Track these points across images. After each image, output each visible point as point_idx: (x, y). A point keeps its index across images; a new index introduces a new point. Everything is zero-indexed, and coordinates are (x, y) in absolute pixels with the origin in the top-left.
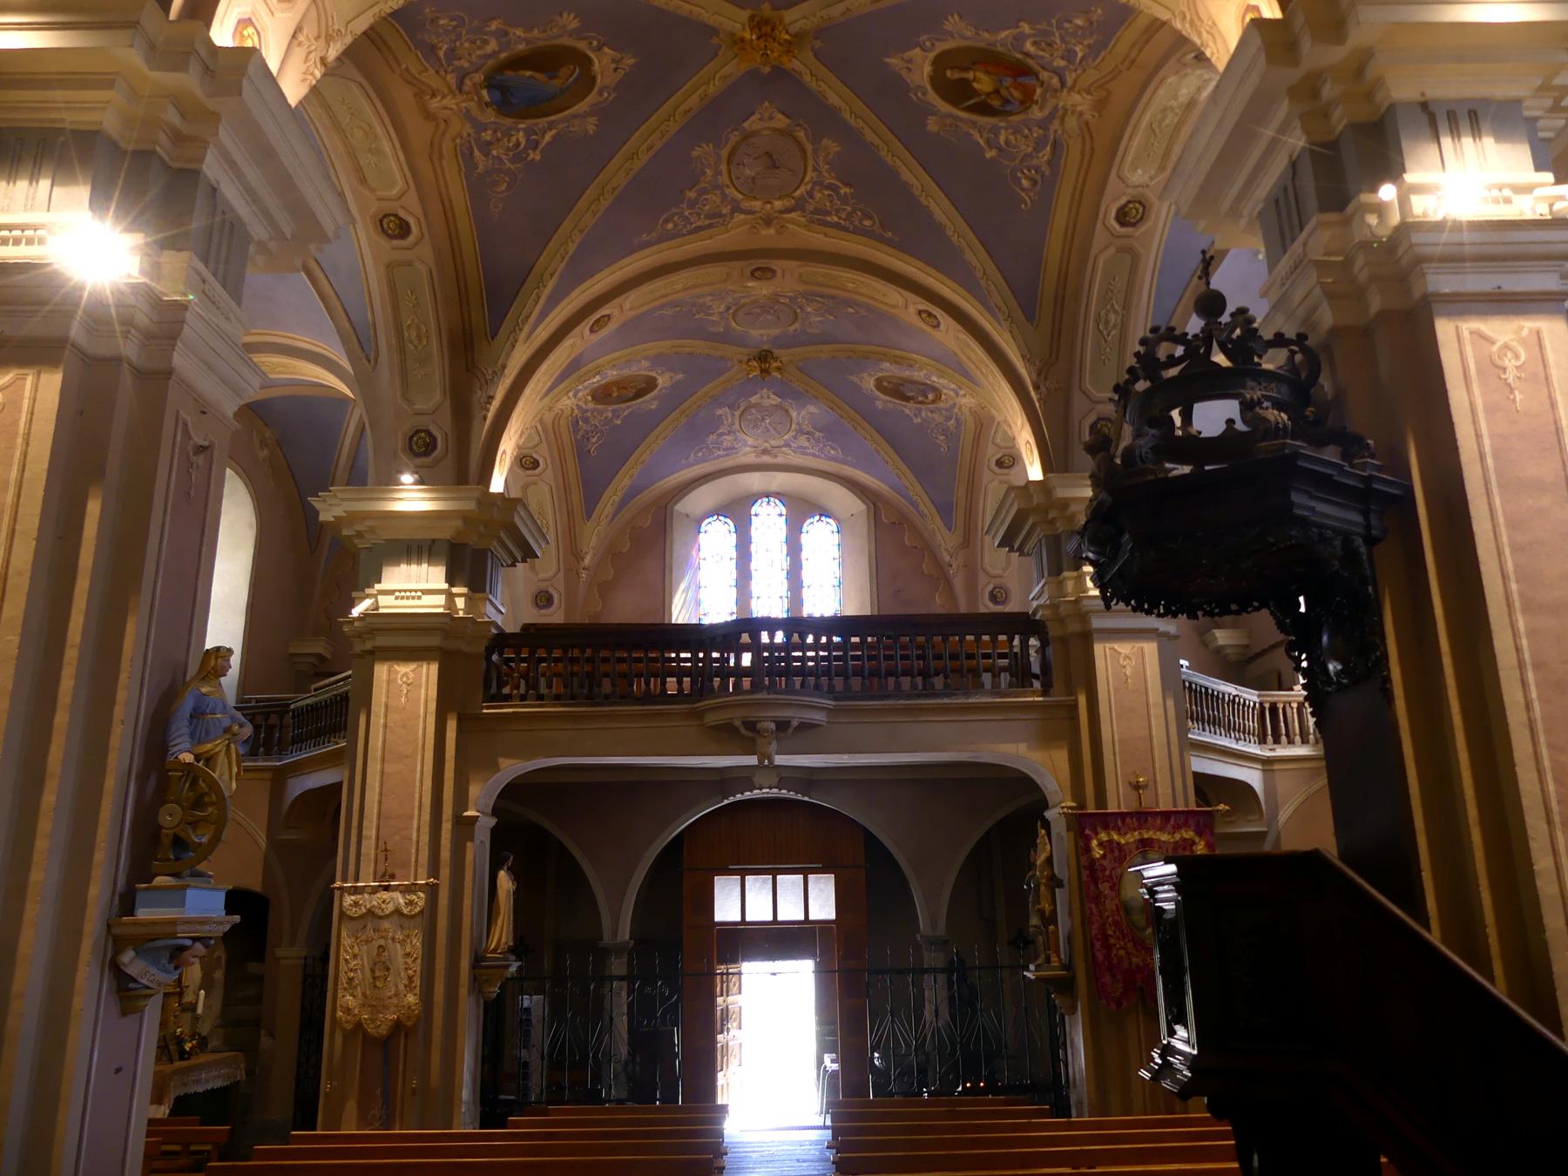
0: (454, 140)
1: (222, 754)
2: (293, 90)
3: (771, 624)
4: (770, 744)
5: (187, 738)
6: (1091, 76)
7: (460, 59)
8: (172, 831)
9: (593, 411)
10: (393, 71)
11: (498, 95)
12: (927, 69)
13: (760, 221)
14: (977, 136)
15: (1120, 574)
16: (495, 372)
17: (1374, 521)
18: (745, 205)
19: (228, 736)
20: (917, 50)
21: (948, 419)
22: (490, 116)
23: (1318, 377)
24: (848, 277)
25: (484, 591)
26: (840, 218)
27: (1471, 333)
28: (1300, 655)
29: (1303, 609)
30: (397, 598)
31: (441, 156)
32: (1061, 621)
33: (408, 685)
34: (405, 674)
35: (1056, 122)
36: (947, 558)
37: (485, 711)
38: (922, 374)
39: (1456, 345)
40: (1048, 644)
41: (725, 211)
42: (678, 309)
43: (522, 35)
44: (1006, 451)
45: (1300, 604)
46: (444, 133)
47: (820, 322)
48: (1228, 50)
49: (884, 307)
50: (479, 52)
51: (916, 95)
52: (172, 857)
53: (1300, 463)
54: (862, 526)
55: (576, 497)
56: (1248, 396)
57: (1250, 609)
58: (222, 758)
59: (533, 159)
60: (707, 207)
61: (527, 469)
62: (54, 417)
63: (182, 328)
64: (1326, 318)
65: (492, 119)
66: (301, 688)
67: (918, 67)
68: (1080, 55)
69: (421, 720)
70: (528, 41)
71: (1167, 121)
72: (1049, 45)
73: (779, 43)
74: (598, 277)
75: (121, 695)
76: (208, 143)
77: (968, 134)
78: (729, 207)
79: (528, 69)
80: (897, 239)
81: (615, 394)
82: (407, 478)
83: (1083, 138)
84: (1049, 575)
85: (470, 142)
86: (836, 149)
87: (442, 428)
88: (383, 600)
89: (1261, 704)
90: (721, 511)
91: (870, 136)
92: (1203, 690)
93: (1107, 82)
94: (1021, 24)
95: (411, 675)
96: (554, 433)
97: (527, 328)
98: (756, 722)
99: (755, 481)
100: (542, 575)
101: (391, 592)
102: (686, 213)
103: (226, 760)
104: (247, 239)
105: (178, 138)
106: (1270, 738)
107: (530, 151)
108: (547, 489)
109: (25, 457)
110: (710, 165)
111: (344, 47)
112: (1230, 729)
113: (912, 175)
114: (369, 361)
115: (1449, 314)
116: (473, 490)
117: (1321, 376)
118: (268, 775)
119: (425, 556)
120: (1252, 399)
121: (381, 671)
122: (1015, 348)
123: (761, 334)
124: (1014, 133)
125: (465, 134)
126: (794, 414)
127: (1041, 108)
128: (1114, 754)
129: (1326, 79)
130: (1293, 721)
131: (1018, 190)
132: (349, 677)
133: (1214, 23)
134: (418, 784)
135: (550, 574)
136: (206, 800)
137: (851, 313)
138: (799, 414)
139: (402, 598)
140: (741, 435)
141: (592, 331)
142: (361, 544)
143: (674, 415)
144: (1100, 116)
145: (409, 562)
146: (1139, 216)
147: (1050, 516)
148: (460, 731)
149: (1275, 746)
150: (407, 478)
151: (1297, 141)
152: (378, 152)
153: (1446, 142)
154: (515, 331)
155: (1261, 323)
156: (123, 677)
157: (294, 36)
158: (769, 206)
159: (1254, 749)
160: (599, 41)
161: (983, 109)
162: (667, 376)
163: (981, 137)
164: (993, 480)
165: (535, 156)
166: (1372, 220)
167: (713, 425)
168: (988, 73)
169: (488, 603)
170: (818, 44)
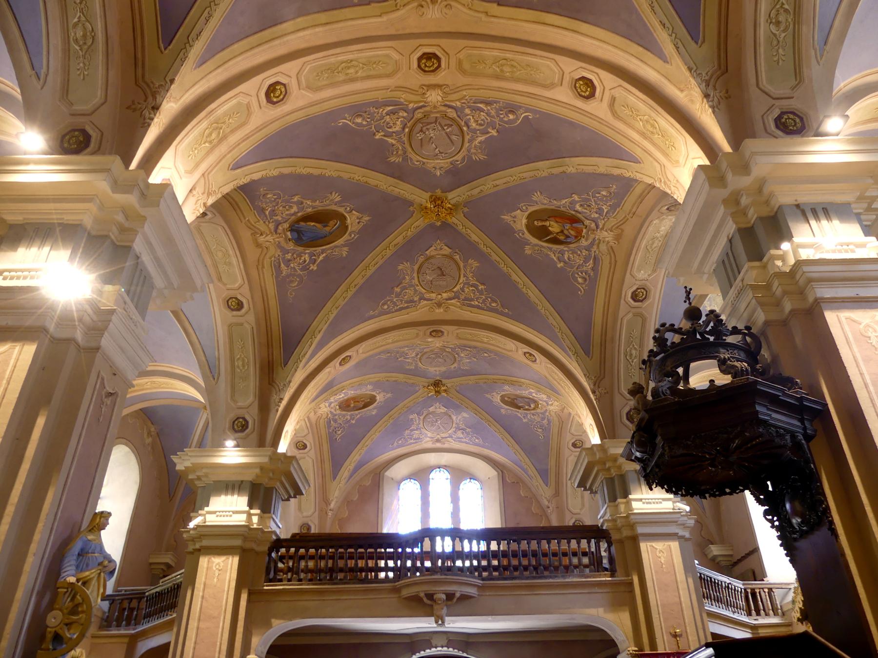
0: (271, 258)
1: (95, 579)
2: (190, 213)
3: (443, 533)
4: (442, 609)
5: (74, 568)
6: (612, 222)
7: (277, 215)
8: (54, 629)
9: (339, 415)
10: (241, 222)
11: (296, 235)
12: (524, 221)
13: (435, 305)
14: (552, 256)
15: (657, 465)
16: (284, 384)
17: (807, 424)
18: (427, 296)
19: (100, 567)
20: (519, 211)
21: (543, 419)
22: (291, 246)
23: (760, 351)
24: (484, 335)
25: (270, 513)
26: (479, 302)
27: (846, 318)
28: (773, 518)
29: (770, 489)
30: (217, 516)
31: (263, 267)
32: (619, 530)
33: (219, 570)
34: (218, 564)
35: (595, 247)
36: (546, 503)
37: (265, 588)
38: (527, 392)
39: (839, 325)
40: (612, 545)
41: (415, 299)
42: (389, 355)
43: (311, 204)
44: (579, 438)
45: (768, 486)
46: (266, 254)
47: (470, 362)
48: (685, 190)
49: (504, 351)
50: (287, 212)
51: (518, 234)
52: (51, 647)
53: (758, 387)
54: (495, 484)
55: (328, 466)
56: (722, 357)
57: (737, 491)
58: (94, 582)
59: (313, 269)
60: (406, 297)
61: (300, 449)
62: (27, 368)
63: (109, 324)
64: (761, 317)
65: (292, 248)
66: (154, 581)
67: (519, 220)
68: (605, 211)
69: (225, 593)
70: (314, 208)
71: (655, 245)
72: (589, 206)
73: (445, 209)
74: (345, 334)
75: (37, 537)
76: (138, 232)
77: (547, 255)
78: (418, 297)
79: (313, 222)
80: (510, 313)
81: (352, 405)
82: (230, 443)
83: (610, 254)
84: (609, 502)
85: (279, 259)
86: (476, 265)
87: (252, 416)
88: (208, 516)
89: (745, 590)
90: (413, 476)
91: (494, 257)
92: (709, 579)
93: (621, 225)
94: (573, 195)
95: (222, 564)
96: (318, 434)
97: (304, 361)
98: (434, 594)
99: (432, 458)
100: (305, 514)
101: (214, 513)
102: (395, 300)
103: (96, 584)
104: (152, 287)
105: (123, 230)
106: (753, 612)
107: (311, 265)
108: (310, 461)
109: (6, 391)
110: (408, 274)
111: (216, 199)
112: (728, 605)
113: (518, 277)
114: (214, 379)
115: (831, 309)
116: (268, 451)
117: (762, 350)
118: (126, 640)
119: (236, 492)
120: (725, 358)
121: (204, 561)
122: (580, 370)
123: (435, 370)
124: (572, 254)
125: (277, 255)
126: (454, 418)
127: (586, 240)
128: (659, 614)
129: (742, 194)
130: (767, 601)
131: (575, 283)
132: (182, 573)
133: (677, 181)
134: (220, 635)
135: (310, 513)
136: (80, 609)
137: (486, 357)
138: (457, 418)
139: (221, 516)
140: (424, 431)
141: (340, 364)
142: (199, 484)
143: (386, 418)
144: (619, 243)
145: (226, 494)
146: (644, 297)
147: (607, 466)
148: (249, 601)
149: (758, 617)
150: (230, 443)
151: (730, 228)
152: (230, 264)
153: (813, 222)
154: (297, 362)
155: (726, 321)
156: (40, 525)
157: (191, 191)
158: (440, 296)
159: (744, 618)
160: (351, 208)
161: (555, 241)
162: (382, 395)
163: (555, 256)
164: (571, 455)
165: (314, 267)
166: (779, 263)
167: (408, 424)
168: (557, 222)
169: (272, 521)
170: (466, 210)
